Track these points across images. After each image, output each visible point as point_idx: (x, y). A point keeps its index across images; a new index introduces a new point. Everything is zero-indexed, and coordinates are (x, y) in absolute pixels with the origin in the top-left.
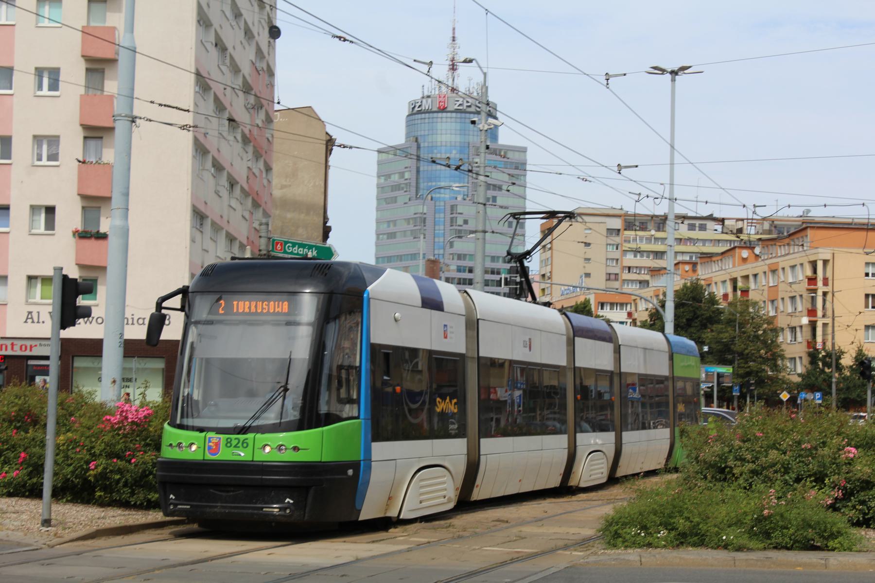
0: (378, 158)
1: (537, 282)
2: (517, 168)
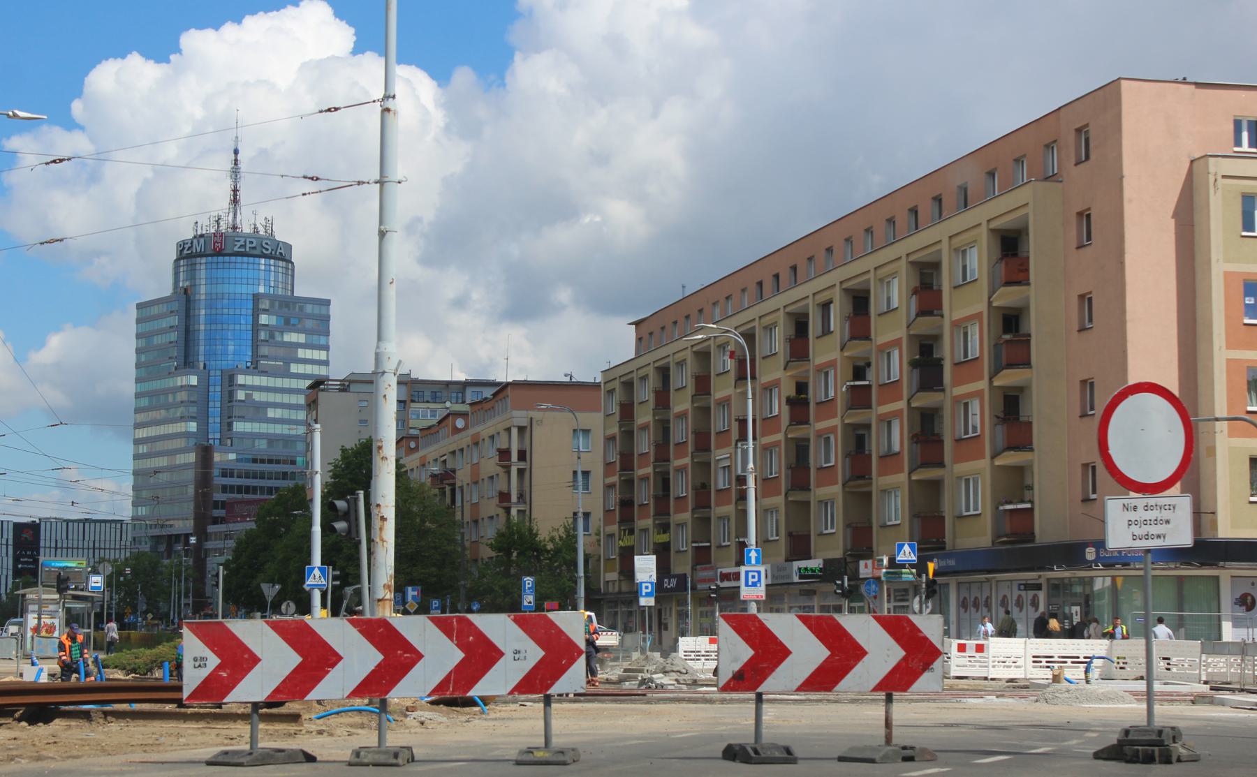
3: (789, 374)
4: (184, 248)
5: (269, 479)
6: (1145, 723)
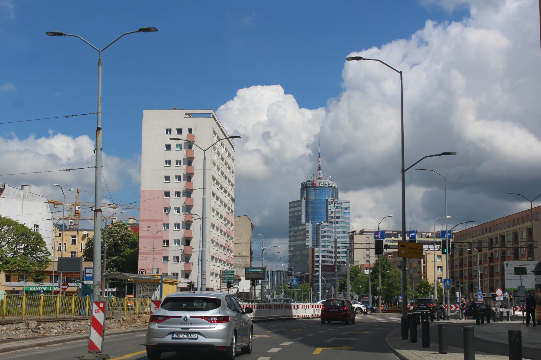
0: (289, 205)
1: (521, 277)
2: (346, 209)
3: (489, 251)
4: (304, 185)
5: (325, 258)
6: (522, 316)
